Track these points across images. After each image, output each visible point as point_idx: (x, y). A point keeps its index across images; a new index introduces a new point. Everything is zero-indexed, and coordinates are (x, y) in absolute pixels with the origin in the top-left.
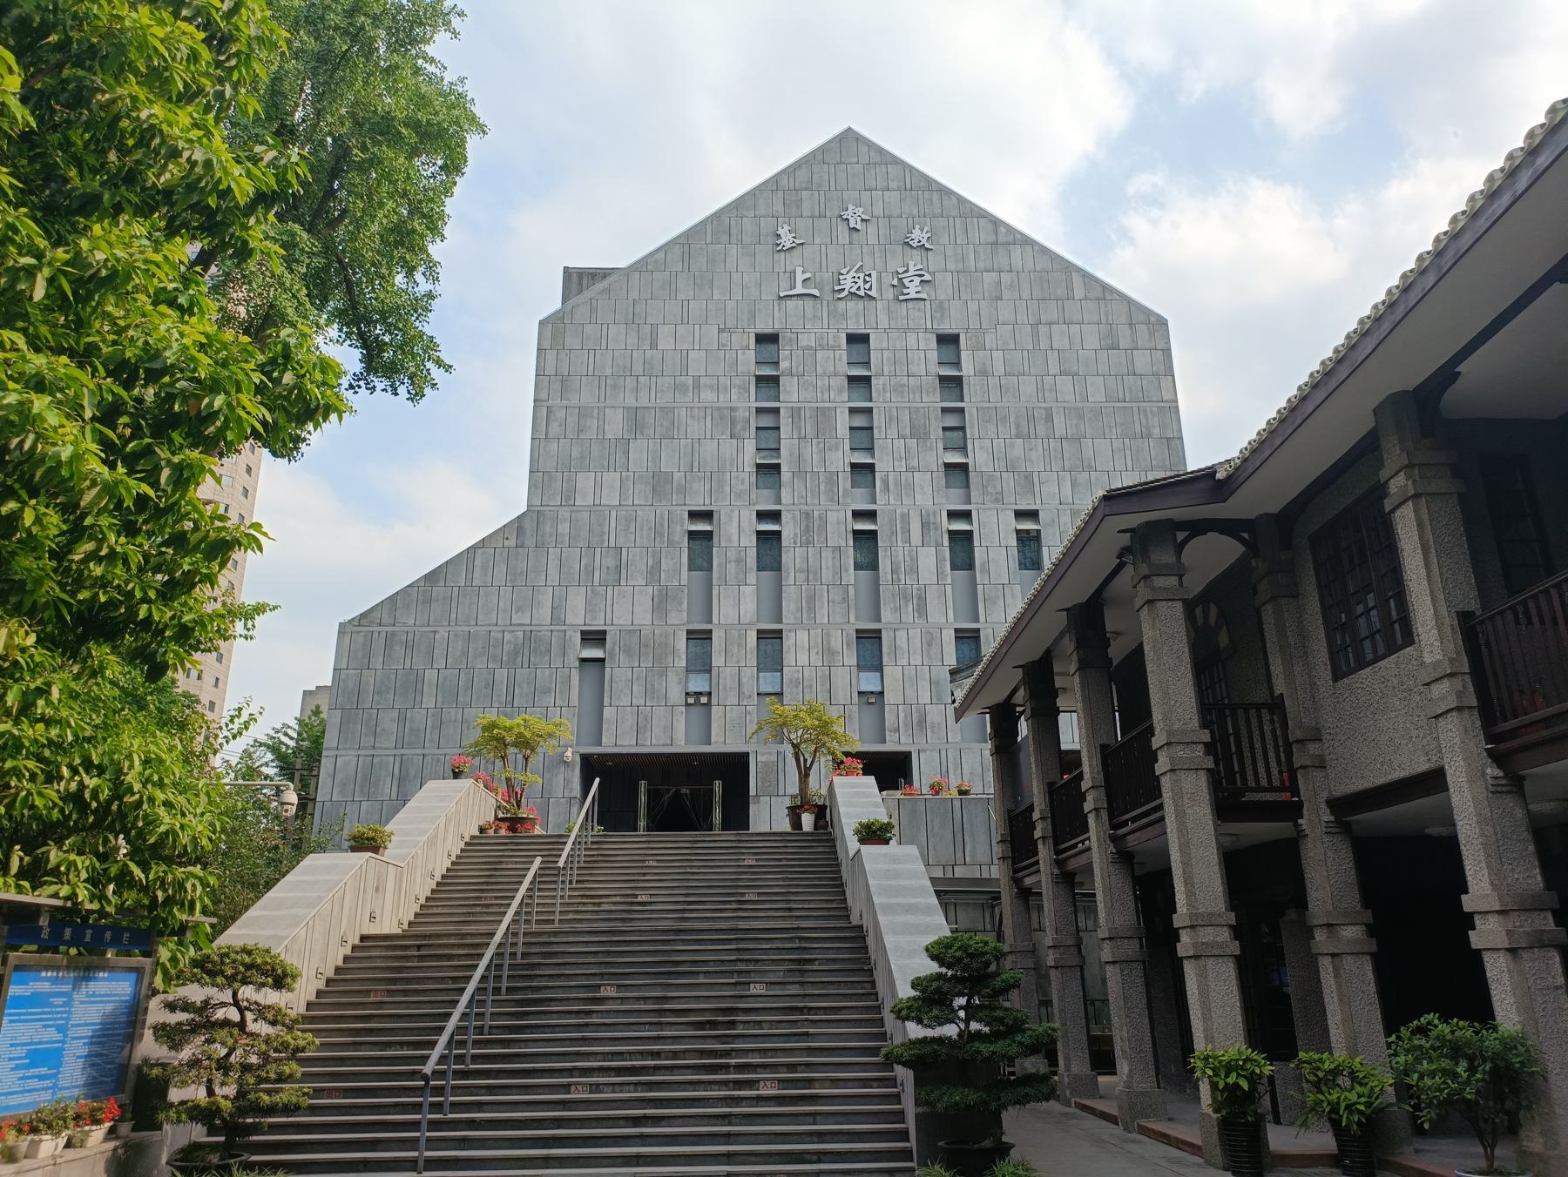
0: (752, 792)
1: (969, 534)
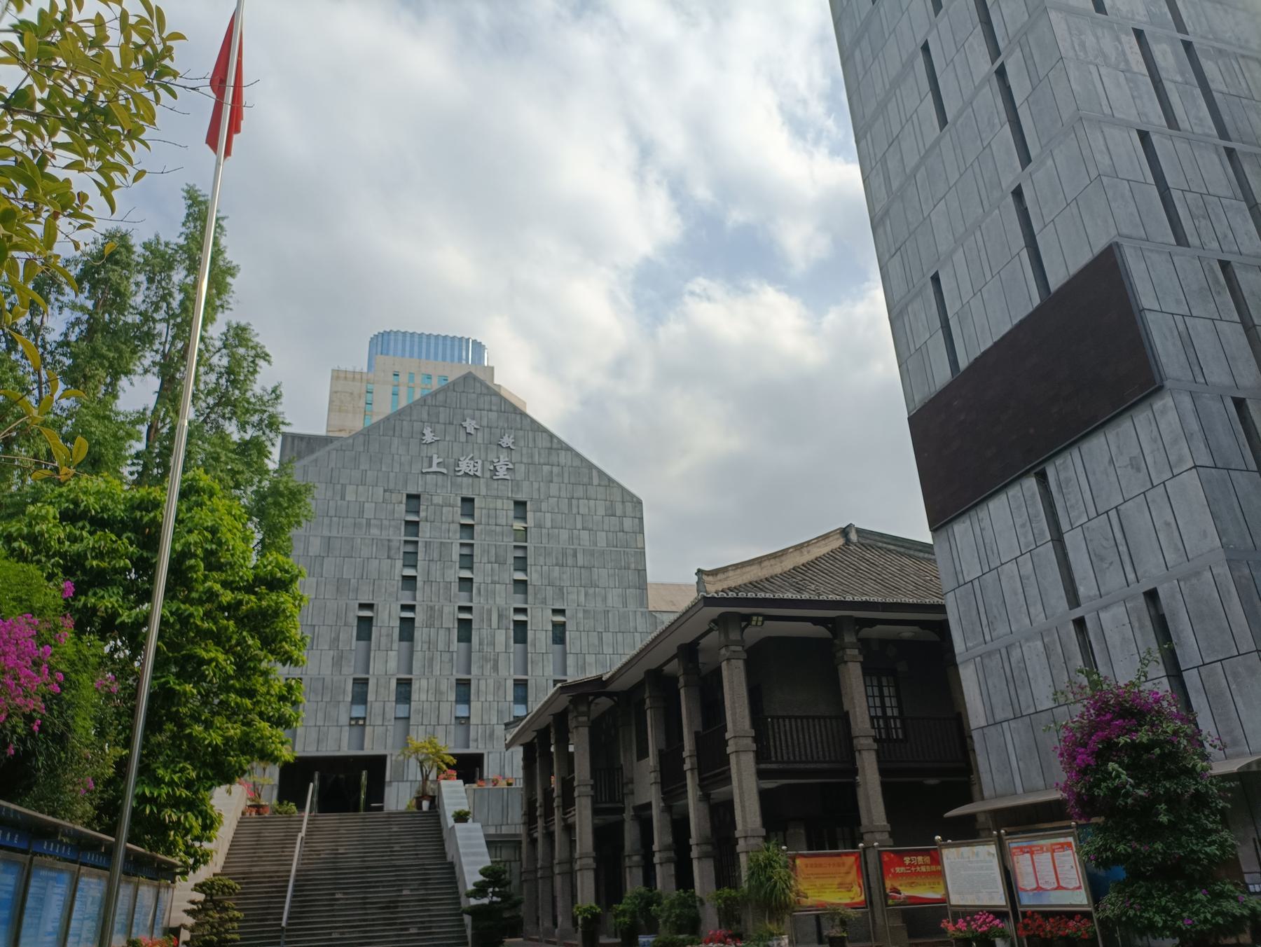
0: (388, 778)
1: (525, 623)
